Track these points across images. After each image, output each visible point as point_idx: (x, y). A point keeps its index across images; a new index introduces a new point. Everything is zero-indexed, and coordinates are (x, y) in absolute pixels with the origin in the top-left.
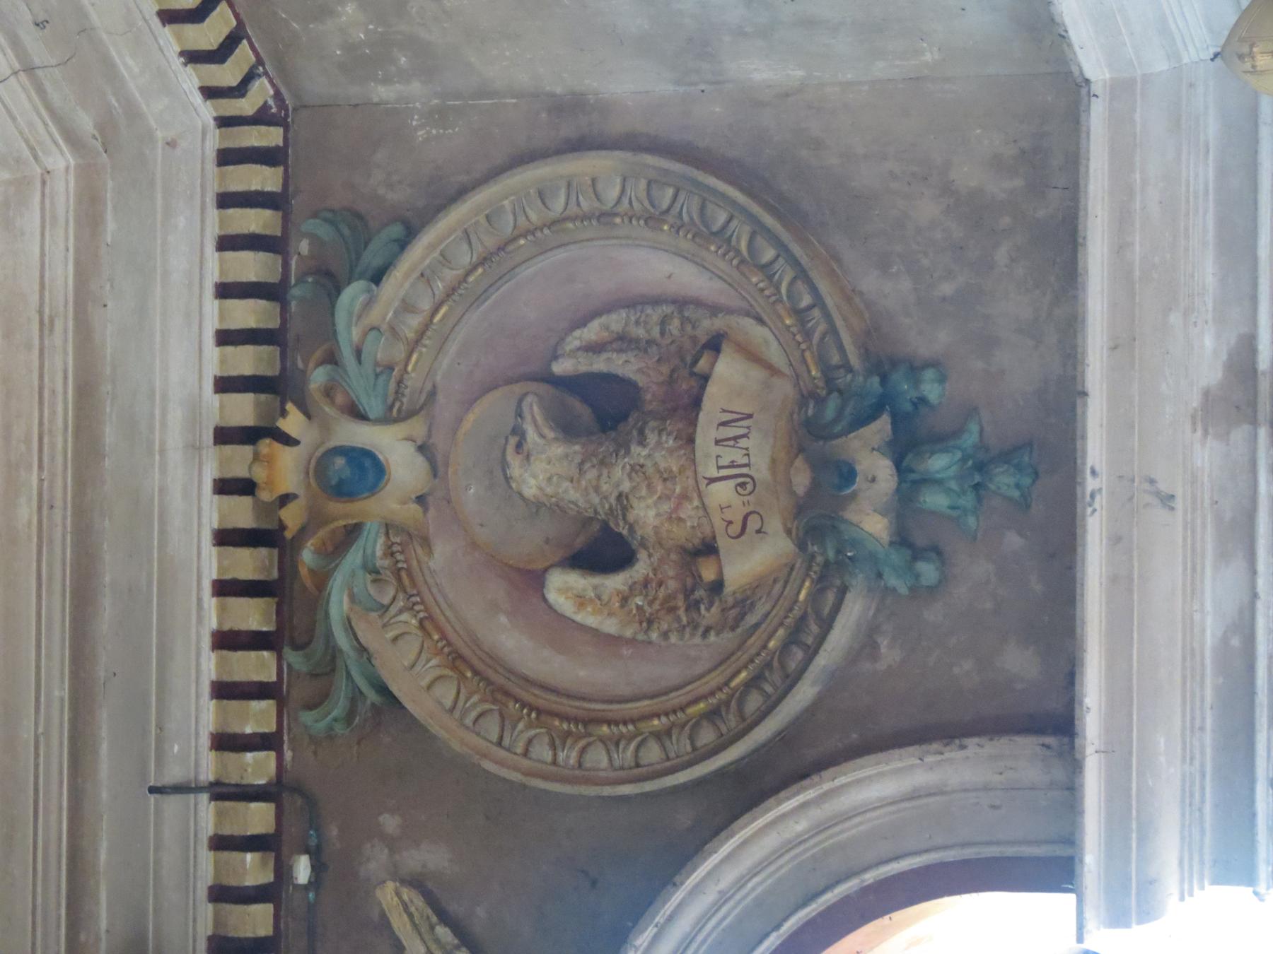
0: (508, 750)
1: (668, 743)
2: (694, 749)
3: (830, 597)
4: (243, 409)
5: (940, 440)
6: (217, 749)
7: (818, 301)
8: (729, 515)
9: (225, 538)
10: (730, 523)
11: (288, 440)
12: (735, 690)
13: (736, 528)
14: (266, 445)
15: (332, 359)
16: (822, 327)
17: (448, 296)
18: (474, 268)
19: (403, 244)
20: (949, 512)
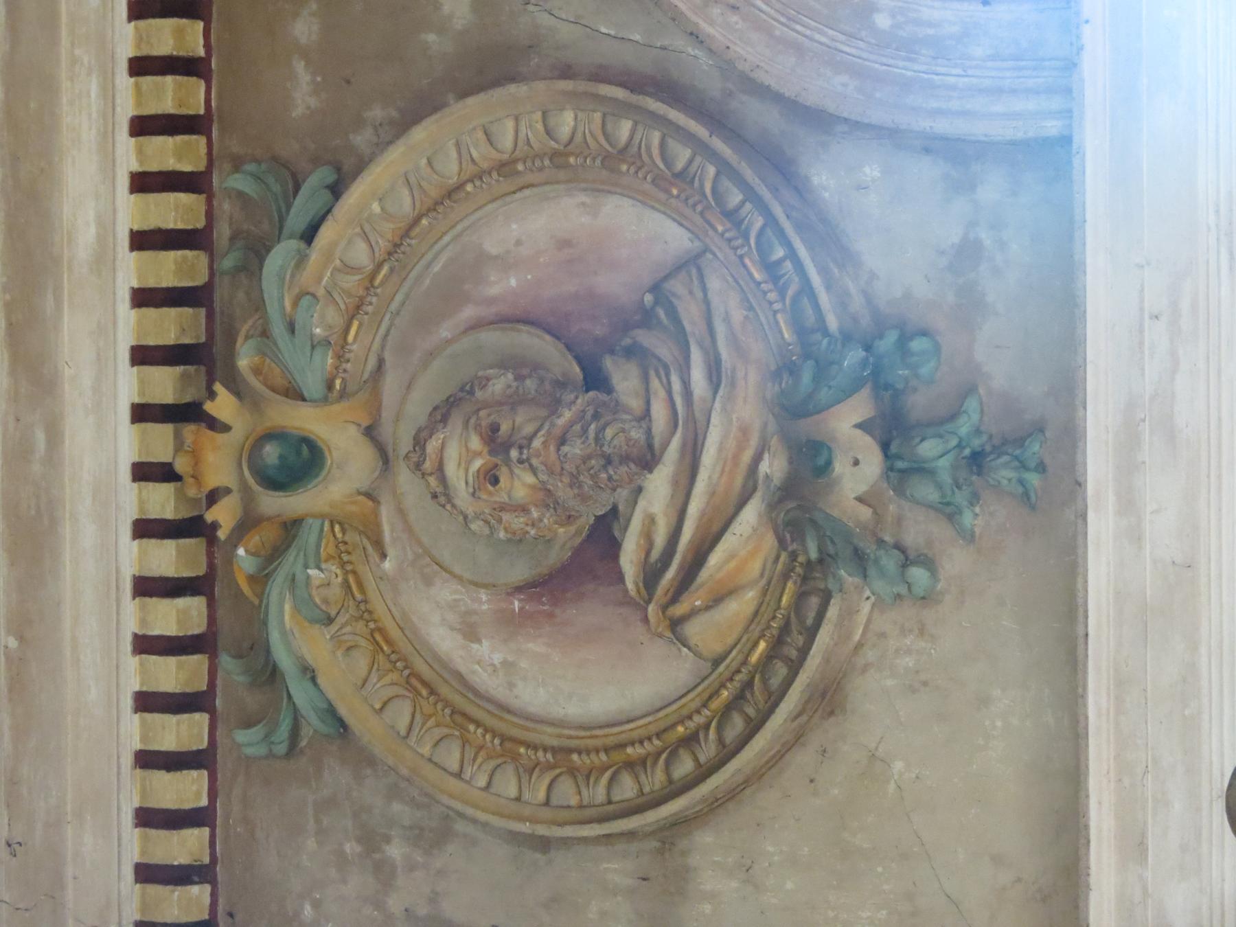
0: (468, 782)
1: (643, 778)
2: (670, 781)
3: (814, 601)
4: (165, 384)
6: (141, 767)
7: (792, 255)
11: (213, 424)
14: (190, 431)
16: (759, 222)
17: (390, 254)
19: (336, 190)
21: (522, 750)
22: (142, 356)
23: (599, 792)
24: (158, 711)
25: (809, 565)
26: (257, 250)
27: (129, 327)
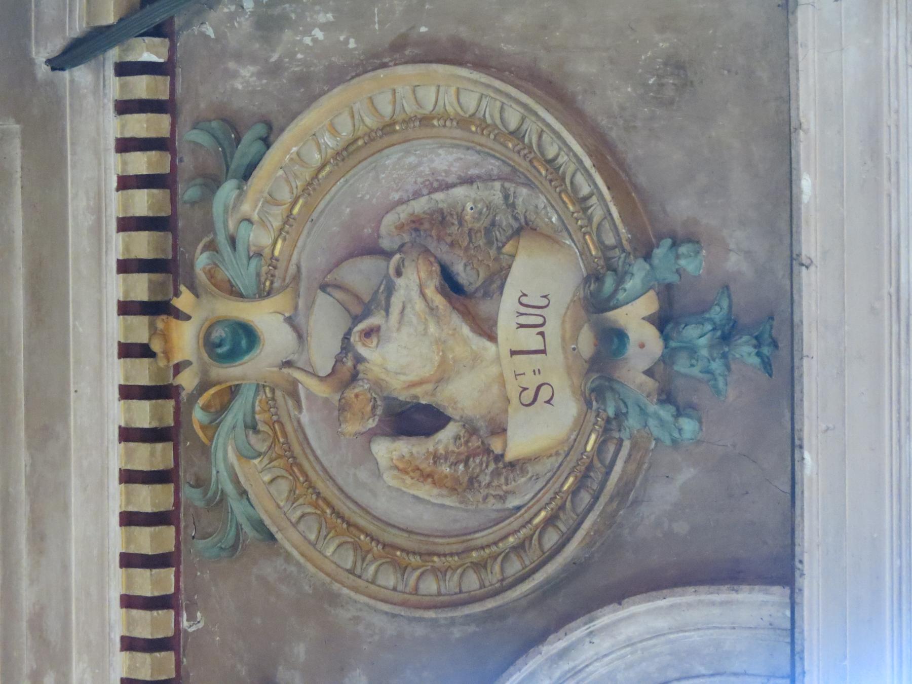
0: (360, 577)
4: (140, 287)
5: (699, 313)
8: (524, 381)
9: (128, 392)
10: (525, 389)
12: (537, 527)
13: (528, 396)
14: (160, 322)
15: (212, 247)
18: (323, 166)
19: (267, 142)
20: (701, 375)
21: (398, 553)
22: (125, 267)
23: (451, 583)
24: (139, 567)
25: (608, 421)
26: (212, 183)
27: (117, 456)
